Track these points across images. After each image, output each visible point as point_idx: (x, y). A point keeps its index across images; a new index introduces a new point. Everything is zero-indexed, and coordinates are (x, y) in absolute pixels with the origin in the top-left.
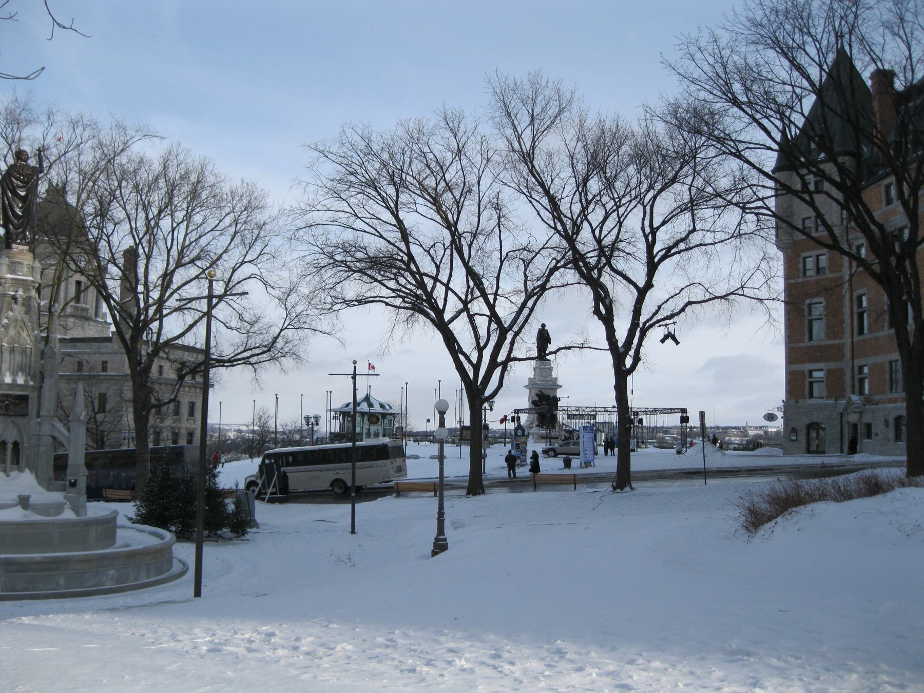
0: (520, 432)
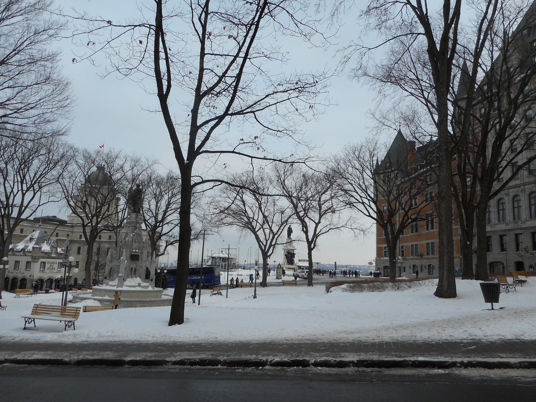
0: (279, 267)
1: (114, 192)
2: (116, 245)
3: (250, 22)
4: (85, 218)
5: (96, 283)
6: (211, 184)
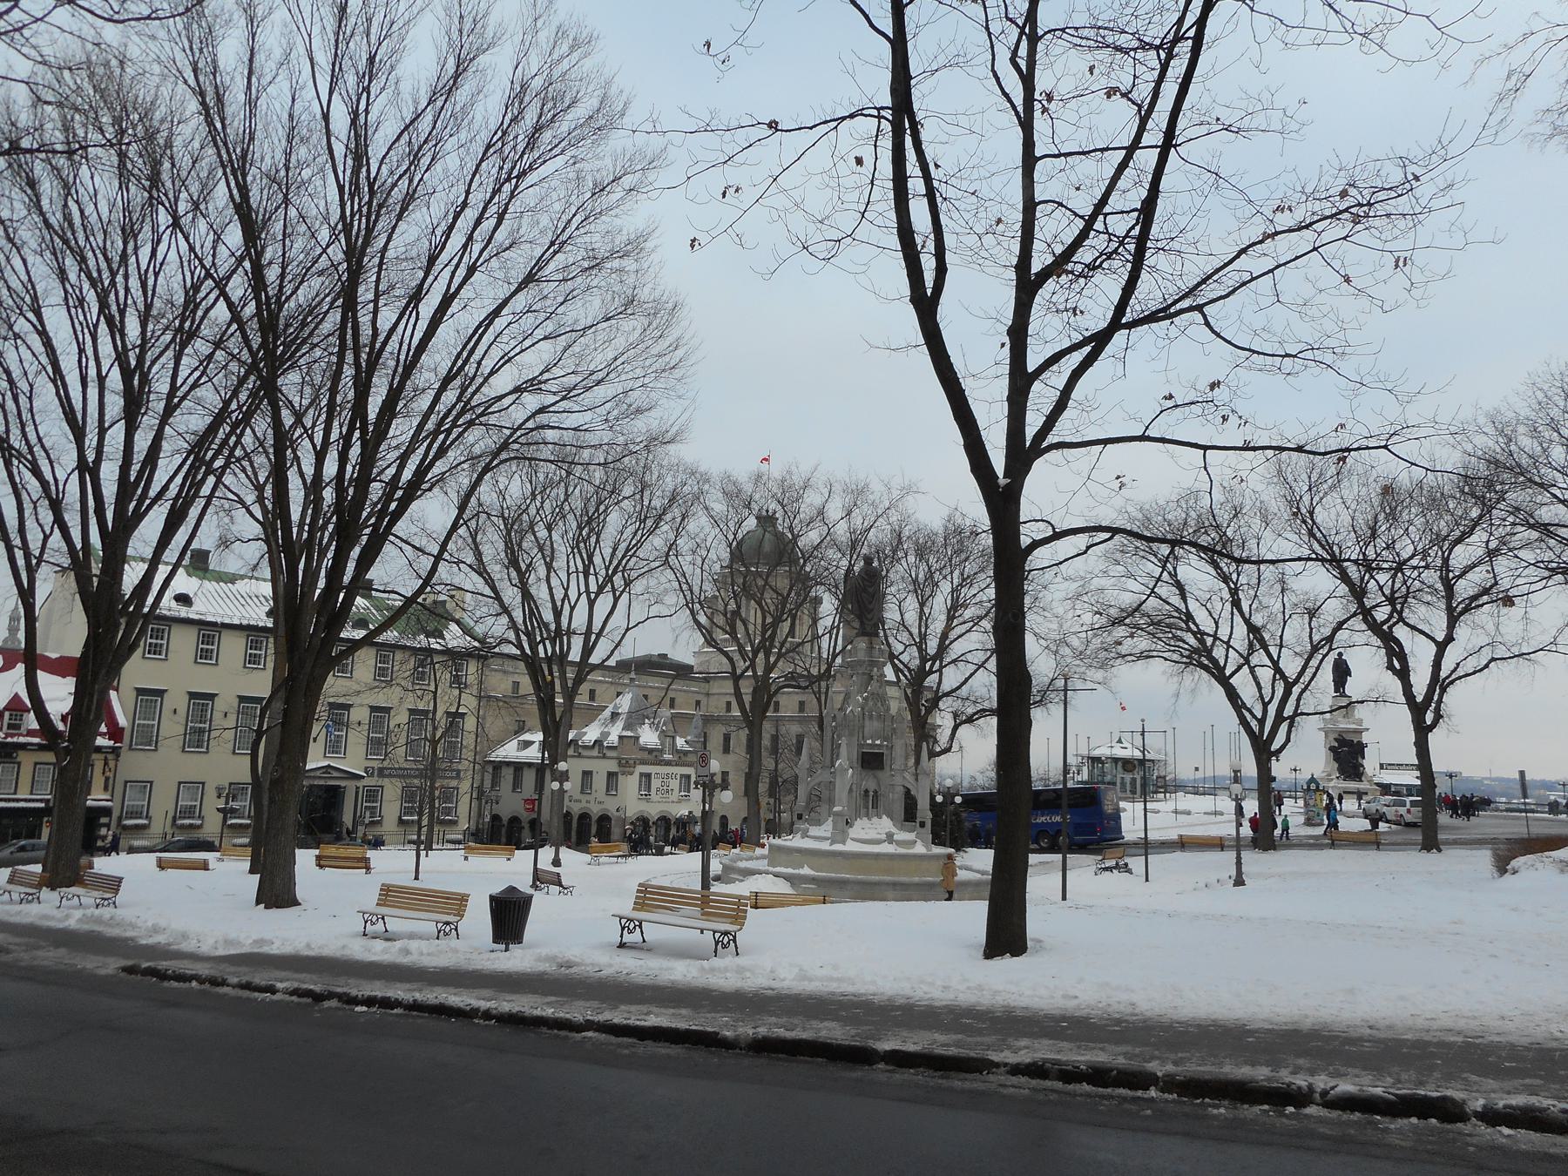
0: (1313, 786)
1: (803, 582)
2: (821, 727)
3: (1170, 37)
4: (736, 657)
5: (774, 829)
6: (1081, 541)
